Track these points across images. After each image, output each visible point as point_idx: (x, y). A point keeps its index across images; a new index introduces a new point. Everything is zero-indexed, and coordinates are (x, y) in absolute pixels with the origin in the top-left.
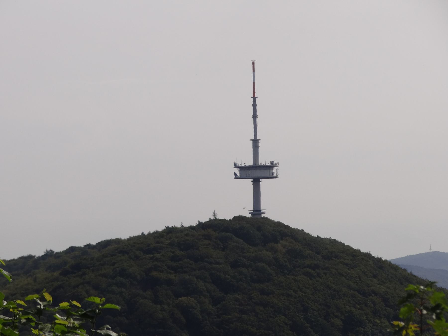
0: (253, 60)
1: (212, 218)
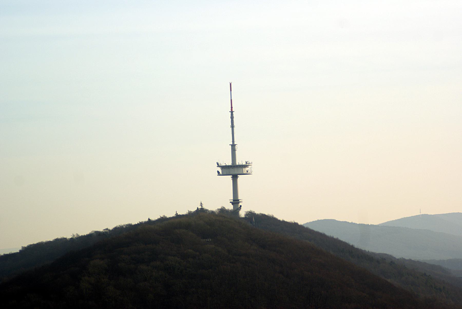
0: (230, 82)
1: (200, 207)
